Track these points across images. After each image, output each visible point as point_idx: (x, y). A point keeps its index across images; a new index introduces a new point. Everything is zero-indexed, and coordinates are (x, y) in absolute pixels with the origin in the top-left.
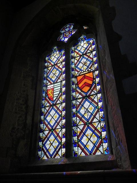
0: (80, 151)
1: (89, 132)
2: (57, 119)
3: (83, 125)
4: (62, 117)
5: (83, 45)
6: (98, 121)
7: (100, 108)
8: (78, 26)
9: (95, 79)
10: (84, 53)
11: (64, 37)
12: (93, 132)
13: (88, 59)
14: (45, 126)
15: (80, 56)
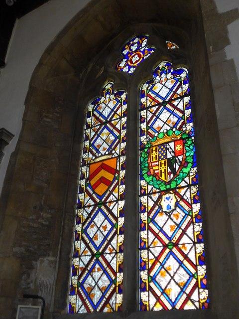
0: (153, 300)
1: (172, 263)
2: (107, 232)
3: (162, 248)
4: (192, 216)
5: (163, 86)
6: (192, 242)
7: (196, 216)
8: (158, 40)
9: (119, 171)
10: (166, 100)
11: (128, 65)
12: (181, 264)
13: (173, 111)
14: (151, 236)
15: (159, 104)
